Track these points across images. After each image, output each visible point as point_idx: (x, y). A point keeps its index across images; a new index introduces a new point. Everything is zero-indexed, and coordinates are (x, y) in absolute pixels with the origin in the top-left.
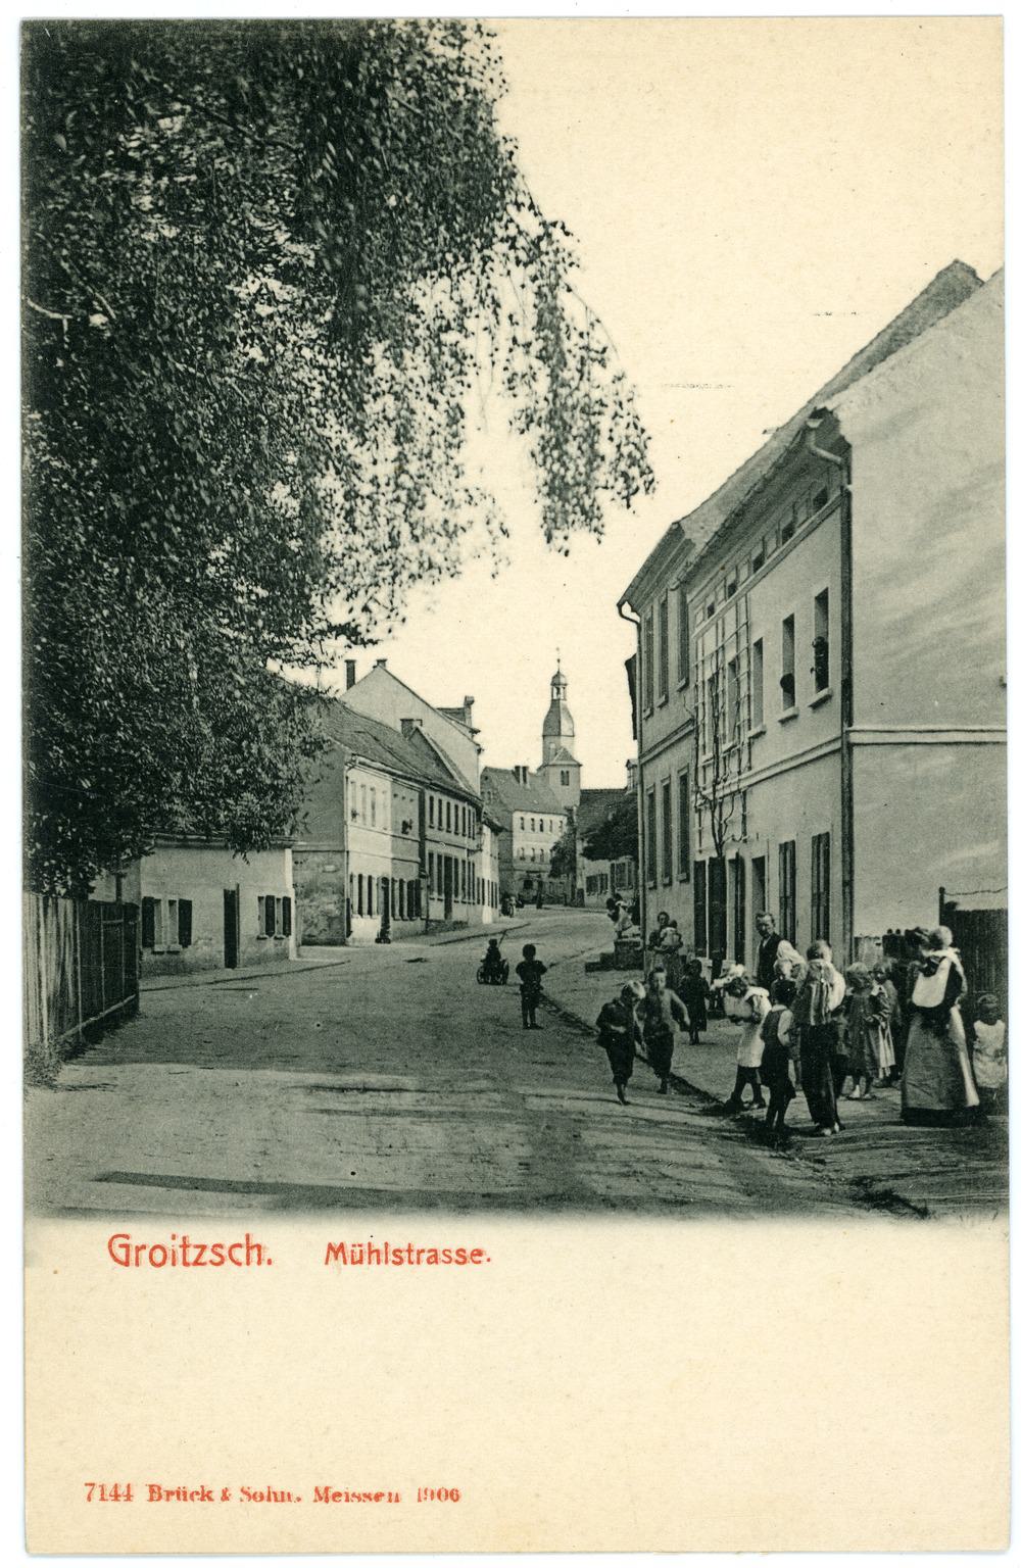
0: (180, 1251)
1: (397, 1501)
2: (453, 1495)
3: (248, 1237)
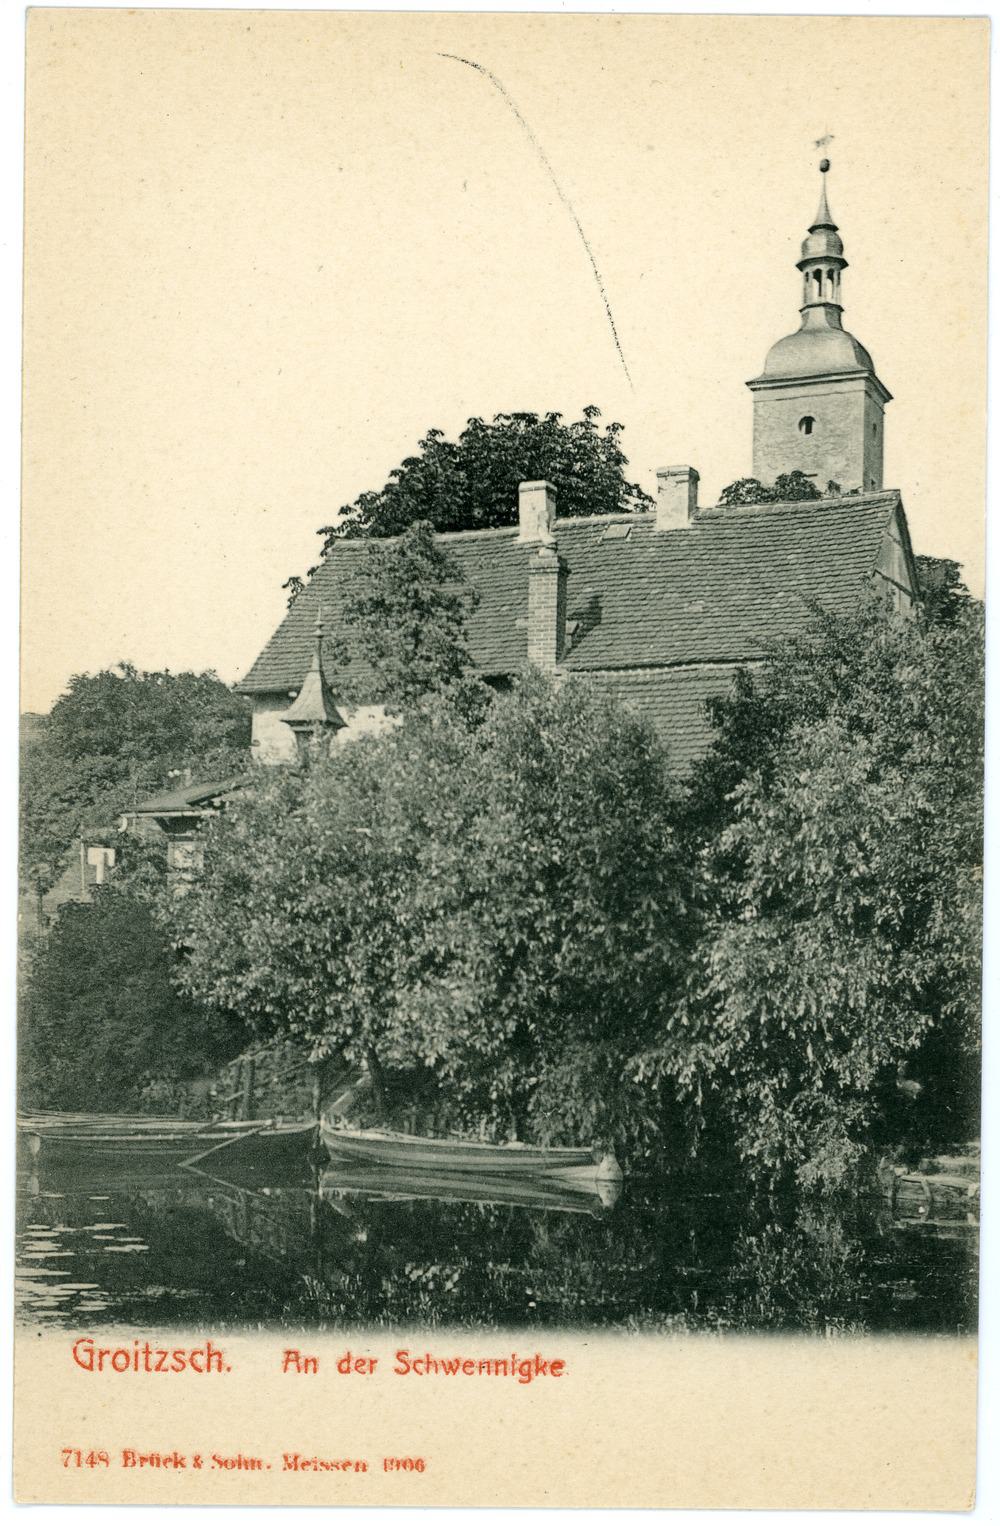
0: (142, 1357)
1: (364, 1470)
2: (418, 1465)
3: (209, 1346)
